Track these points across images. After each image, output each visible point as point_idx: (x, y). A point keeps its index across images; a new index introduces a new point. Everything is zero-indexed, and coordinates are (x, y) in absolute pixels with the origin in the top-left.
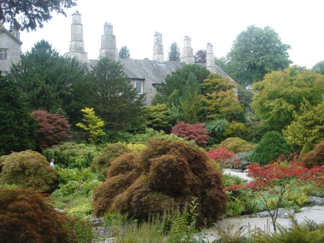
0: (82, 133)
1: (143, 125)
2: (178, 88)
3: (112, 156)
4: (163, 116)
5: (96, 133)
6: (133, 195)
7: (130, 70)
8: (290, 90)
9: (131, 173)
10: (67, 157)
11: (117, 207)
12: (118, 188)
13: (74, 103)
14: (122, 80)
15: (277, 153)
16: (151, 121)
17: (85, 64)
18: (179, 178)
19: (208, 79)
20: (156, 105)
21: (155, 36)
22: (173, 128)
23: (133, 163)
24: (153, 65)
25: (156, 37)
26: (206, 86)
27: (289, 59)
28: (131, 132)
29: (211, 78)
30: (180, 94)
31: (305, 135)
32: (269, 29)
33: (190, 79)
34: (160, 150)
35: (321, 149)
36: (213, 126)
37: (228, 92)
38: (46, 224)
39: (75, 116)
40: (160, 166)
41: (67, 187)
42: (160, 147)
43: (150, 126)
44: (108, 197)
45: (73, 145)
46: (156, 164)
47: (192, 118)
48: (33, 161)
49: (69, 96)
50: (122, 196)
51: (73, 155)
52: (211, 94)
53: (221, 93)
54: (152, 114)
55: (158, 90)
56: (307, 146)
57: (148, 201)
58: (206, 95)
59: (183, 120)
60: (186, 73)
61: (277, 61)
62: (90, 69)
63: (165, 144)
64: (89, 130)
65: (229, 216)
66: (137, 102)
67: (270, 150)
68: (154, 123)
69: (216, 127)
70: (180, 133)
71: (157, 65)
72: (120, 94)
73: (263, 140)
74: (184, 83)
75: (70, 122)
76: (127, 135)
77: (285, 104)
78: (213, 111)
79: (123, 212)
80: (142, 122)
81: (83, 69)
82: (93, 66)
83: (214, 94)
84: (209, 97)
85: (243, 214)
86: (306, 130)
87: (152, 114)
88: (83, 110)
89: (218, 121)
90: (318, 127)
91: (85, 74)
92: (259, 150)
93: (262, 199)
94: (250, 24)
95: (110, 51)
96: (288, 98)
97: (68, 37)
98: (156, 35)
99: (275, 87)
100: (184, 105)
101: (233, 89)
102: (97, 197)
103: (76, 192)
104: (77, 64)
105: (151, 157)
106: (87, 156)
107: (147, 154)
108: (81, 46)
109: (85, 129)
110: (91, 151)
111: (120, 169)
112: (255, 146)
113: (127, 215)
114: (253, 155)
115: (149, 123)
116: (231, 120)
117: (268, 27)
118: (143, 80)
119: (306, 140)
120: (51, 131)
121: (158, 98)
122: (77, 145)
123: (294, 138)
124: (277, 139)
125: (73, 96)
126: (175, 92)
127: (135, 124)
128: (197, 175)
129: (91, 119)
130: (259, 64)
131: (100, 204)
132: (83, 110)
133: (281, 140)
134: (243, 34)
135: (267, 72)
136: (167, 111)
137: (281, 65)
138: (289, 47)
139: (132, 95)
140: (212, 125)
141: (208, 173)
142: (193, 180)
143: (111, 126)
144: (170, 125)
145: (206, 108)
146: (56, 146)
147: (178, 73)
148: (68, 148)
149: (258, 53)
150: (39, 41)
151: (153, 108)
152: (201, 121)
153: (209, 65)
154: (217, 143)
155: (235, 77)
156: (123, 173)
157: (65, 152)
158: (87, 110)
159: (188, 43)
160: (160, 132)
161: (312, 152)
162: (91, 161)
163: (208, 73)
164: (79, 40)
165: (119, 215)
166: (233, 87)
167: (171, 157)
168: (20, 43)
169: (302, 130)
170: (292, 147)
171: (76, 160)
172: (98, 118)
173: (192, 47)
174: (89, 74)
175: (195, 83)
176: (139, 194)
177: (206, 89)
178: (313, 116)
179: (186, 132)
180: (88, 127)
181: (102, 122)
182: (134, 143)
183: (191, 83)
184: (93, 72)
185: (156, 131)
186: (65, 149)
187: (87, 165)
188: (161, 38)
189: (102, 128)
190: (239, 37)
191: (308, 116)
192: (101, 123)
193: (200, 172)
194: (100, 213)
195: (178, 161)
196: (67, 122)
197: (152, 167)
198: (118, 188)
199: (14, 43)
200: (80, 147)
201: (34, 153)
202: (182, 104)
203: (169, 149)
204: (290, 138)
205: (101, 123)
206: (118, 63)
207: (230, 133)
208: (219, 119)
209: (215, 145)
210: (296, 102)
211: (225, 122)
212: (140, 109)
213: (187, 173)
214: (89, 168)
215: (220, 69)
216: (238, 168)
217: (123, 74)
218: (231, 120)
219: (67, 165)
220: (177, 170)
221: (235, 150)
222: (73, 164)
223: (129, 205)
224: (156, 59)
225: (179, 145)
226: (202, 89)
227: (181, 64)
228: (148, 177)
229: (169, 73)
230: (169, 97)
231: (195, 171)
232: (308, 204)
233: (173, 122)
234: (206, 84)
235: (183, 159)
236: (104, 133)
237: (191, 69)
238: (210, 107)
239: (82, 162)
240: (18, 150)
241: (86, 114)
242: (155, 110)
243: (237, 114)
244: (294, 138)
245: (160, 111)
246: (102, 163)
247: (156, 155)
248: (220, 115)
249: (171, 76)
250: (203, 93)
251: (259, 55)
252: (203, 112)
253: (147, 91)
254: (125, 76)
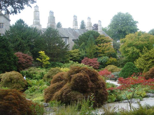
0: (39, 63)
1: (68, 59)
2: (84, 42)
3: (53, 74)
4: (78, 55)
5: (46, 63)
6: (63, 92)
7: (62, 33)
8: (138, 43)
9: (62, 82)
10: (32, 74)
11: (56, 98)
12: (56, 89)
13: (35, 49)
14: (58, 38)
15: (131, 72)
16: (72, 57)
17: (41, 30)
18: (85, 84)
19: (99, 38)
20: (74, 50)
21: (74, 17)
22: (82, 60)
23: (63, 77)
24: (73, 31)
25: (74, 18)
26: (98, 41)
27: (137, 28)
28: (62, 62)
29: (101, 37)
30: (86, 44)
31: (145, 64)
32: (128, 14)
33: (91, 38)
34: (76, 71)
35: (152, 70)
36: (101, 60)
37: (109, 43)
38: (22, 106)
39: (36, 55)
40: (76, 79)
41: (32, 89)
42: (76, 70)
43: (71, 60)
44: (51, 93)
45: (35, 69)
46: (74, 77)
47: (91, 56)
48: (16, 76)
49: (33, 45)
50: (58, 93)
51: (35, 73)
52: (100, 44)
53: (105, 44)
54: (72, 54)
55: (75, 42)
56: (146, 69)
57: (70, 95)
58: (98, 45)
59: (87, 57)
60: (88, 35)
61: (132, 29)
62: (43, 33)
63: (78, 68)
64: (42, 62)
65: (109, 102)
66: (65, 48)
67: (128, 71)
68: (73, 58)
69: (103, 60)
70: (86, 63)
71: (74, 31)
72: (57, 45)
73: (125, 66)
74: (87, 39)
75: (33, 58)
76: (60, 64)
77: (135, 49)
78: (101, 52)
79: (58, 100)
80: (67, 58)
81: (40, 33)
82: (44, 31)
83: (102, 44)
84: (99, 46)
85: (115, 101)
86: (146, 62)
87: (72, 54)
88: (39, 52)
89: (104, 57)
90: (151, 60)
91: (41, 35)
92: (123, 71)
93: (125, 94)
94: (119, 11)
95: (52, 24)
96: (137, 46)
97: (32, 18)
98: (74, 17)
99: (131, 41)
100: (88, 50)
101: (111, 42)
102: (46, 93)
103: (36, 91)
104: (37, 30)
105: (72, 74)
106: (42, 74)
107: (70, 73)
108: (38, 22)
109: (41, 61)
110: (43, 72)
111: (57, 80)
112: (121, 69)
113: (60, 102)
114: (120, 73)
115: (71, 58)
116: (110, 57)
117: (127, 13)
118: (68, 38)
119: (146, 66)
120: (24, 62)
121: (75, 46)
122: (36, 69)
123: (140, 65)
124: (131, 66)
125: (34, 45)
126: (83, 43)
127: (64, 59)
128: (94, 83)
129: (43, 56)
130: (123, 30)
131: (48, 97)
132: (39, 52)
133: (133, 66)
134: (116, 16)
135: (127, 34)
136: (79, 53)
137: (134, 31)
138: (137, 22)
139: (63, 45)
140: (101, 59)
141: (99, 82)
142: (92, 85)
143: (53, 60)
144: (81, 59)
145: (98, 51)
146: (26, 69)
147: (85, 34)
148: (32, 70)
149: (122, 25)
150: (19, 19)
151: (73, 51)
152: (95, 57)
153: (100, 31)
154: (103, 68)
155: (111, 36)
156: (58, 82)
157: (31, 72)
158: (41, 52)
159: (89, 20)
160: (76, 62)
161: (148, 72)
162: (43, 76)
163: (99, 34)
164: (38, 19)
165: (56, 102)
166: (111, 41)
167: (81, 74)
168: (10, 21)
169: (144, 62)
170: (139, 70)
171: (36, 76)
172: (47, 56)
173: (91, 22)
174: (42, 35)
175: (93, 39)
176: (66, 92)
177: (98, 42)
178: (149, 55)
179: (89, 63)
180: (42, 60)
181: (49, 58)
182: (64, 68)
183: (91, 39)
184: (44, 34)
185: (74, 62)
186: (31, 70)
187: (41, 78)
188: (77, 18)
189: (48, 60)
190: (114, 17)
191: (147, 55)
192: (48, 58)
193: (95, 82)
194: (47, 101)
195: (85, 76)
196: (32, 58)
197: (72, 79)
198: (56, 89)
199: (7, 21)
200: (38, 70)
201: (16, 73)
202: (86, 49)
203: (80, 71)
204: (138, 65)
205: (48, 58)
206: (56, 30)
207: (109, 63)
208: (104, 56)
209: (102, 69)
210: (141, 48)
211: (107, 58)
212: (66, 51)
213: (89, 82)
214: (42, 79)
215: (105, 33)
216: (113, 80)
217: (59, 35)
218: (110, 57)
219: (32, 78)
220: (84, 80)
221: (112, 71)
222: (35, 78)
223: (61, 97)
224: (74, 28)
225: (85, 69)
226: (96, 42)
227: (86, 30)
228: (70, 84)
229: (80, 34)
230: (81, 46)
231: (93, 81)
232: (146, 97)
233: (82, 58)
234: (98, 40)
235: (87, 75)
236: (49, 63)
237: (91, 32)
238: (100, 51)
239: (39, 77)
240: (8, 71)
241: (41, 54)
242: (74, 52)
243: (113, 54)
244: (140, 65)
245: (76, 52)
246: (49, 77)
247: (74, 73)
248: (105, 54)
249: (81, 36)
250: (96, 44)
251: (123, 26)
252: (96, 53)
253: (70, 43)
254: (59, 36)
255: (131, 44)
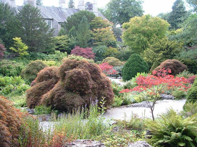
0: (13, 54)
1: (53, 49)
2: (75, 25)
4: (66, 43)
5: (23, 54)
6: (54, 95)
7: (45, 14)
8: (145, 28)
9: (51, 80)
10: (5, 69)
11: (44, 102)
12: (43, 90)
13: (7, 34)
14: (39, 19)
15: (138, 67)
16: (58, 46)
17: (14, 8)
18: (84, 84)
19: (94, 20)
20: (61, 36)
22: (72, 50)
23: (52, 73)
24: (59, 10)
26: (93, 25)
28: (45, 53)
29: (97, 19)
30: (77, 29)
31: (154, 57)
33: (83, 20)
34: (72, 66)
35: (164, 65)
36: (97, 50)
37: (107, 28)
38: (10, 118)
40: (72, 76)
41: (6, 89)
42: (71, 64)
43: (57, 49)
44: (37, 96)
45: (8, 61)
46: (70, 74)
47: (84, 45)
49: (4, 30)
50: (47, 95)
52: (96, 29)
53: (103, 29)
54: (59, 41)
55: (62, 26)
56: (155, 63)
57: (64, 98)
58: (93, 30)
59: (78, 45)
60: (80, 16)
61: (136, 10)
62: (18, 12)
63: (75, 62)
64: (18, 52)
65: (113, 107)
66: (49, 33)
67: (134, 65)
68: (60, 47)
69: (99, 50)
70: (77, 54)
71: (61, 10)
72: (38, 29)
73: (129, 59)
74: (79, 22)
75: (6, 47)
76: (43, 55)
77: (142, 37)
78: (97, 40)
79: (48, 105)
81: (13, 12)
82: (20, 10)
83: (98, 30)
84: (95, 31)
85: (122, 105)
86: (155, 54)
87: (59, 41)
88: (14, 39)
89: (101, 47)
90: (162, 52)
91: (15, 15)
92: (127, 66)
93: (131, 96)
96: (144, 33)
99: (137, 26)
100: (79, 36)
101: (110, 27)
102: (29, 96)
103: (13, 92)
104: (9, 8)
105: (66, 70)
107: (63, 68)
110: (20, 66)
111: (42, 79)
112: (124, 63)
113: (50, 107)
114: (124, 68)
115: (57, 47)
116: (108, 46)
118: (52, 19)
119: (155, 59)
121: (62, 31)
122: (11, 62)
123: (148, 58)
124: (138, 59)
125: (6, 29)
126: (74, 27)
127: (48, 48)
128: (95, 81)
129: (19, 45)
130: (125, 12)
131: (32, 100)
133: (141, 59)
135: (130, 17)
137: (139, 13)
139: (46, 29)
140: (97, 49)
141: (102, 80)
142: (93, 84)
143: (33, 49)
145: (93, 38)
147: (75, 15)
148: (5, 63)
151: (59, 38)
152: (89, 46)
153: (95, 11)
154: (99, 60)
155: (110, 19)
156: (46, 80)
158: (17, 39)
160: (64, 53)
161: (159, 67)
162: (21, 72)
163: (94, 16)
165: (45, 107)
166: (110, 25)
167: (80, 70)
169: (153, 54)
170: (147, 64)
171: (11, 71)
174: (17, 15)
175: (86, 22)
176: (59, 94)
177: (93, 27)
178: (159, 45)
179: (81, 53)
180: (17, 50)
181: (27, 47)
182: (47, 60)
183: (84, 22)
184: (20, 14)
185: (62, 53)
187: (18, 75)
189: (26, 50)
191: (157, 45)
192: (26, 47)
193: (97, 80)
194: (32, 106)
195: (84, 73)
196: (3, 46)
197: (66, 77)
198: (43, 90)
200: (13, 63)
202: (77, 35)
203: (78, 65)
204: (145, 58)
205: (26, 47)
206: (37, 8)
207: (108, 54)
208: (101, 45)
209: (98, 62)
210: (148, 35)
211: (105, 47)
212: (51, 38)
213: (89, 80)
214: (20, 76)
215: (101, 14)
216: (114, 76)
217: (40, 16)
218: (108, 46)
219: (5, 74)
220: (84, 79)
221: (112, 64)
222: (9, 74)
223: (52, 100)
224: (60, 6)
225: (84, 62)
226: (91, 26)
227: (76, 10)
228: (64, 83)
229: (69, 15)
230: (70, 31)
231: (94, 79)
232: (161, 98)
233: (72, 47)
235: (87, 71)
236: (28, 54)
237: (84, 13)
238: (96, 38)
239: (14, 73)
242: (61, 39)
243: (112, 42)
244: (148, 58)
245: (62, 39)
246: (28, 72)
247: (69, 68)
248: (102, 43)
249: (71, 17)
250: (91, 29)
252: (91, 41)
253: (55, 27)
254: (41, 17)
255: (136, 29)
